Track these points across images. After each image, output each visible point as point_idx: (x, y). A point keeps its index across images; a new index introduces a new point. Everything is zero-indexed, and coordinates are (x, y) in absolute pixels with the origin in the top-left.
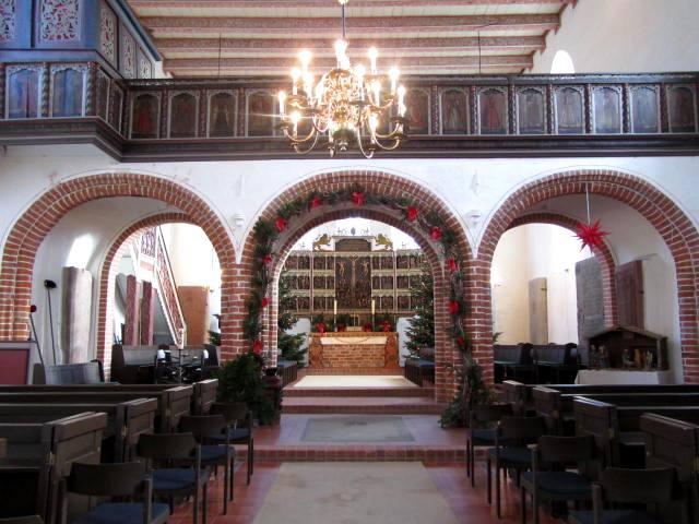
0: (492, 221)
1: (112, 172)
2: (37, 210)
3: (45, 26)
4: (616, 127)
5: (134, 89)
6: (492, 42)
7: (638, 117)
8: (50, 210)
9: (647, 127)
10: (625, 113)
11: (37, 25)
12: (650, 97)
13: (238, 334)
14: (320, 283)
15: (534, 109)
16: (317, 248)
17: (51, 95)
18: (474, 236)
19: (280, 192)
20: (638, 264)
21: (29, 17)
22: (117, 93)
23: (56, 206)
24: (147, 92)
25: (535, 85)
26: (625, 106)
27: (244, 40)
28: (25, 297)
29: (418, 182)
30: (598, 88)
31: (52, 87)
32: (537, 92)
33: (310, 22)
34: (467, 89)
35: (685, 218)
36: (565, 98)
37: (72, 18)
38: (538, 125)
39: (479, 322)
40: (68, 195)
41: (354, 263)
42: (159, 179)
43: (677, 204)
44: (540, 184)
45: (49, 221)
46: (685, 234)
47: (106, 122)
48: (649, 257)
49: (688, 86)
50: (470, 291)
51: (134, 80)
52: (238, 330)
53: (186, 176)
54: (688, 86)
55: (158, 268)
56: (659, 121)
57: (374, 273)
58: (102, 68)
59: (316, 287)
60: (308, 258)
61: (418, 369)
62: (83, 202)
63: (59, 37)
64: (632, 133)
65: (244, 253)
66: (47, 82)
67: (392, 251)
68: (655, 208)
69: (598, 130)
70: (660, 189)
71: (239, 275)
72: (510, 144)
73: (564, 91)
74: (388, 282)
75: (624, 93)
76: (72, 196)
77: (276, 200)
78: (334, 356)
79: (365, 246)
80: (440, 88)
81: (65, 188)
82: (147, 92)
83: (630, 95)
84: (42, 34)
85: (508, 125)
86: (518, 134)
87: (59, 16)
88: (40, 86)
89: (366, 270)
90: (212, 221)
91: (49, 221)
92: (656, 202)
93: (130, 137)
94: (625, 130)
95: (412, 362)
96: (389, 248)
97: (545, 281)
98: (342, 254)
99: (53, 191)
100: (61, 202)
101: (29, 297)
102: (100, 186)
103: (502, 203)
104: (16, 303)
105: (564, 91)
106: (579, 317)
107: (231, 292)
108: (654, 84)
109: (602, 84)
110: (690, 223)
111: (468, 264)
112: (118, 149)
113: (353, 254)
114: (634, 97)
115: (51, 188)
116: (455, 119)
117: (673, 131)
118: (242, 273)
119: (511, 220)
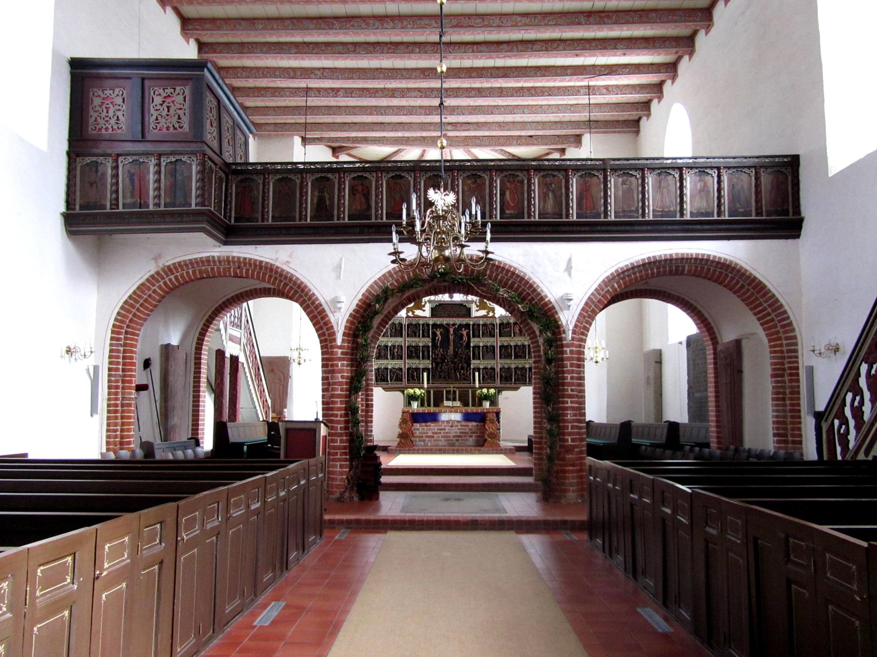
1: (216, 254)
3: (154, 117)
5: (236, 172)
6: (604, 91)
7: (733, 199)
9: (741, 210)
10: (719, 198)
11: (147, 119)
12: (746, 180)
13: (339, 413)
14: (413, 352)
15: (628, 192)
16: (410, 314)
17: (162, 185)
18: (568, 318)
20: (738, 343)
21: (140, 109)
22: (220, 178)
23: (160, 287)
24: (248, 176)
25: (631, 169)
26: (719, 190)
27: (333, 89)
28: (131, 376)
29: (514, 265)
30: (693, 172)
31: (163, 176)
32: (632, 175)
33: (404, 73)
34: (563, 173)
36: (660, 182)
37: (181, 109)
38: (633, 209)
40: (172, 277)
41: (452, 330)
42: (261, 262)
44: (633, 268)
45: (154, 303)
46: (777, 316)
47: (212, 209)
48: (748, 336)
49: (783, 169)
50: (563, 372)
51: (233, 164)
52: (340, 409)
53: (288, 259)
54: (783, 169)
55: (244, 341)
56: (753, 203)
57: (474, 342)
58: (210, 159)
59: (410, 357)
60: (401, 325)
61: (401, 442)
62: (187, 282)
63: (168, 128)
65: (344, 335)
66: (159, 172)
67: (493, 317)
68: (748, 290)
69: (692, 214)
70: (754, 273)
71: (339, 355)
72: (604, 228)
73: (659, 174)
74: (489, 351)
75: (719, 176)
76: (176, 278)
77: (375, 282)
78: (430, 434)
79: (464, 312)
80: (536, 172)
81: (169, 270)
82: (248, 176)
83: (725, 178)
84: (152, 125)
85: (603, 209)
86: (612, 218)
87: (168, 107)
88: (152, 177)
89: (465, 338)
90: (313, 303)
91: (154, 303)
92: (749, 284)
94: (719, 214)
96: (491, 314)
97: (660, 351)
98: (438, 321)
99: (158, 273)
100: (165, 283)
101: (134, 376)
102: (203, 268)
103: (596, 286)
104: (123, 382)
105: (659, 174)
106: (689, 394)
107: (333, 372)
108: (749, 167)
110: (781, 306)
112: (223, 233)
113: (451, 321)
114: (729, 180)
115: (156, 270)
116: (550, 202)
117: (767, 216)
118: (342, 353)
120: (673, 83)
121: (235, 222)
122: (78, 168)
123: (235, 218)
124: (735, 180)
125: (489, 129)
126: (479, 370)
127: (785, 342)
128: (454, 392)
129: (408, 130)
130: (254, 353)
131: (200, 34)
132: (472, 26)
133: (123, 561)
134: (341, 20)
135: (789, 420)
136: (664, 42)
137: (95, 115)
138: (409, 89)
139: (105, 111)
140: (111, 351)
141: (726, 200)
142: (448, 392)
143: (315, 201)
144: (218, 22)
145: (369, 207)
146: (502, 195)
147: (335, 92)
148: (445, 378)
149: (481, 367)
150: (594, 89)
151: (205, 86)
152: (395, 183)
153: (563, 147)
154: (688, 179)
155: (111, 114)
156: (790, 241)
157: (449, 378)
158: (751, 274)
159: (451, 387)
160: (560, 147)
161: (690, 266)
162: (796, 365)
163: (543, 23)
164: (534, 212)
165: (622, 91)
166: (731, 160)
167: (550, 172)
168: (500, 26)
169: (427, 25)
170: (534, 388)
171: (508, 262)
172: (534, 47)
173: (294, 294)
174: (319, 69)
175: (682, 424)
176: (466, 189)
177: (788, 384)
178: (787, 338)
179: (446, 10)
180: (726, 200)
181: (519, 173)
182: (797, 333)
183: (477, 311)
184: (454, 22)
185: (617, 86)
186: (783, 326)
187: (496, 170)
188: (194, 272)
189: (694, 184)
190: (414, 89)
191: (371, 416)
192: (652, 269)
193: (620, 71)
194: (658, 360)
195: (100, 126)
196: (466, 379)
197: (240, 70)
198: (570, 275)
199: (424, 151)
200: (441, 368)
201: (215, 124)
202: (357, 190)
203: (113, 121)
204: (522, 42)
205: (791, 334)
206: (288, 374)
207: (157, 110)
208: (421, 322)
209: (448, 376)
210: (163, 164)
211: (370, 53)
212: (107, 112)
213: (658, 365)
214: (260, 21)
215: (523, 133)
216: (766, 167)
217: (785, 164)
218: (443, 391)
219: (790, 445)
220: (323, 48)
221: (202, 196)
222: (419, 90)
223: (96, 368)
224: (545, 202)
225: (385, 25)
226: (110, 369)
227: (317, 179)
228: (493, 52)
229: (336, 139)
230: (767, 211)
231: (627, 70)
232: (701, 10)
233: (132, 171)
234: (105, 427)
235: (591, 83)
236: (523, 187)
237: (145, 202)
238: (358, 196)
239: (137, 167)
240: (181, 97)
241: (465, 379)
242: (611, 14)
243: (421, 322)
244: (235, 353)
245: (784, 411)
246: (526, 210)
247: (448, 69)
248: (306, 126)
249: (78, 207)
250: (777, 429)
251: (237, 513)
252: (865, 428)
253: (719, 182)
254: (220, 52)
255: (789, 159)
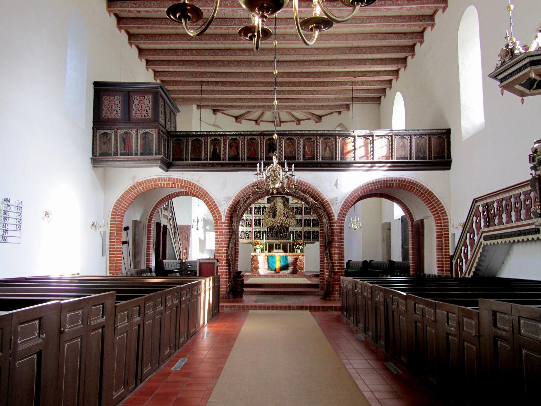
0: (345, 202)
2: (126, 195)
4: (406, 156)
6: (361, 84)
7: (418, 151)
8: (132, 195)
9: (422, 156)
18: (335, 210)
19: (244, 187)
20: (422, 221)
23: (135, 193)
24: (179, 138)
27: (215, 82)
29: (310, 183)
33: (254, 75)
35: (439, 201)
39: (337, 250)
40: (141, 187)
43: (435, 194)
46: (439, 208)
49: (442, 136)
58: (162, 131)
59: (256, 225)
64: (414, 160)
65: (226, 217)
75: (411, 139)
76: (143, 188)
77: (241, 191)
83: (413, 140)
92: (426, 192)
93: (171, 160)
94: (410, 158)
95: (440, 275)
97: (390, 223)
99: (134, 186)
100: (137, 191)
108: (425, 135)
109: (400, 135)
111: (333, 223)
114: (416, 141)
115: (133, 184)
116: (328, 151)
117: (434, 159)
119: (356, 199)
120: (412, 58)
121: (172, 161)
122: (98, 135)
123: (172, 158)
124: (418, 141)
125: (299, 102)
126: (293, 232)
127: (443, 221)
128: (280, 245)
129: (255, 102)
130: (174, 223)
131: (129, 28)
132: (290, 55)
133: (125, 323)
134: (222, 51)
135: (444, 260)
136: (391, 61)
137: (105, 109)
138: (256, 82)
139: (110, 107)
140: (111, 224)
141: (414, 151)
142: (276, 245)
143: (212, 151)
144: (158, 51)
145: (238, 154)
146: (304, 148)
147: (217, 83)
148: (274, 237)
149: (295, 231)
150: (355, 83)
151: (159, 95)
152: (251, 142)
153: (340, 110)
154: (396, 141)
155: (113, 109)
156: (446, 171)
157: (277, 237)
158: (426, 188)
159: (278, 242)
160: (338, 110)
161: (396, 184)
162: (447, 232)
163: (327, 53)
164: (320, 157)
165: (370, 83)
166: (417, 131)
167: (327, 137)
168: (304, 55)
169: (267, 54)
170: (320, 243)
171: (307, 181)
172: (323, 64)
173: (199, 195)
174: (209, 72)
175: (397, 262)
176: (286, 144)
177: (444, 242)
178: (444, 219)
179: (277, 47)
180: (414, 151)
181: (312, 137)
182: (448, 217)
183: (292, 200)
184: (281, 52)
185: (367, 81)
186: (442, 213)
187: (301, 136)
188: (152, 185)
189: (398, 143)
190: (259, 82)
191: (238, 257)
192: (377, 185)
193: (368, 75)
194: (389, 228)
195: (108, 115)
196: (286, 237)
197: (167, 73)
198: (337, 188)
199: (263, 113)
200: (272, 231)
201: (163, 113)
202: (232, 145)
203: (115, 112)
204: (316, 61)
205: (445, 217)
206: (190, 235)
207: (136, 107)
208: (262, 206)
209: (276, 235)
210: (139, 134)
211: (237, 66)
212: (112, 108)
213: (388, 230)
214: (179, 51)
215: (318, 104)
216: (434, 134)
217: (443, 133)
218: (273, 244)
219: (445, 272)
220: (212, 63)
221: (158, 149)
222: (262, 83)
223: (105, 233)
224: (325, 152)
225: (245, 54)
226: (111, 233)
227: (213, 140)
228: (301, 66)
229: (216, 106)
230: (434, 157)
231: (372, 74)
232: (409, 46)
233: (124, 137)
234: (108, 262)
235: (354, 80)
236: (314, 144)
237: (130, 152)
238: (233, 148)
239: (127, 135)
240: (148, 101)
241: (285, 237)
242: (362, 48)
243: (262, 206)
244: (166, 224)
245: (442, 255)
246: (315, 156)
247: (278, 73)
248: (201, 99)
249: (98, 155)
250: (439, 264)
251: (169, 304)
252: (468, 262)
253: (411, 142)
254: (157, 65)
255: (446, 131)
